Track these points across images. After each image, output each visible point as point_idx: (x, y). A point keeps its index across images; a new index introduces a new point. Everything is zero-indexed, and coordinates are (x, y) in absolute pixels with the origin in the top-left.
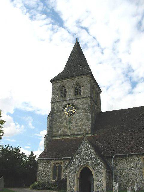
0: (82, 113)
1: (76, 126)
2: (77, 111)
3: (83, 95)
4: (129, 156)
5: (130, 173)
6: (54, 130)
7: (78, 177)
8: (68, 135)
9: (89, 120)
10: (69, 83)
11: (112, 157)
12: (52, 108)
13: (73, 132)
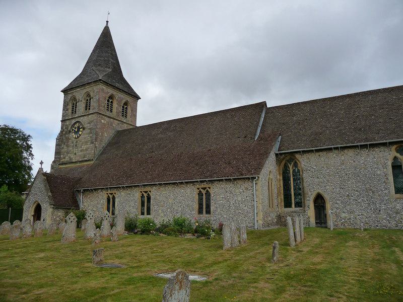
1: (81, 151)
2: (84, 132)
4: (95, 190)
5: (94, 209)
6: (62, 156)
7: (33, 214)
8: (73, 163)
12: (62, 128)
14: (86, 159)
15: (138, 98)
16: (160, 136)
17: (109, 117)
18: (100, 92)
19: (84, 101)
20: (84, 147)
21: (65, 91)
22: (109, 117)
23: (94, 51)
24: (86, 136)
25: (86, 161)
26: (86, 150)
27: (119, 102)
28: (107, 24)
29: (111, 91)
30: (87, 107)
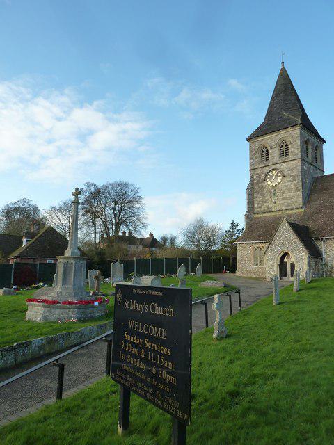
1: (283, 199)
3: (291, 157)
11: (322, 239)
19: (278, 148)
20: (286, 195)
26: (291, 198)
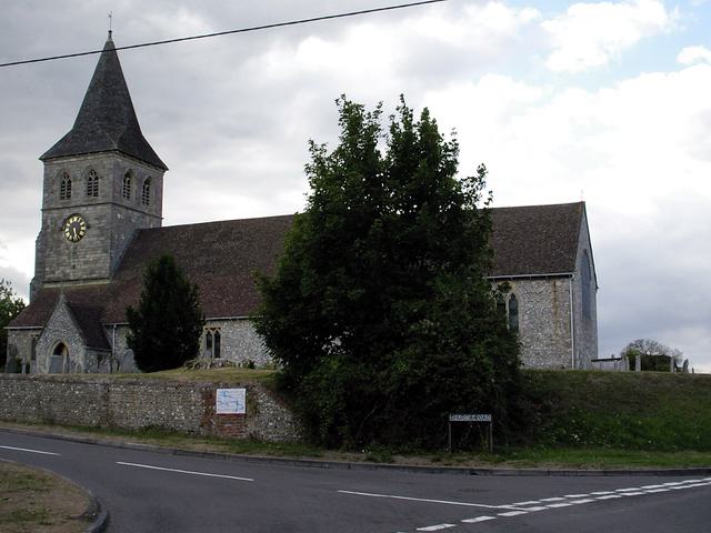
0: (94, 236)
1: (85, 263)
2: (89, 232)
3: (100, 199)
6: (47, 269)
9: (106, 252)
10: (76, 166)
12: (44, 222)
13: (79, 274)
14: (94, 276)
15: (165, 168)
16: (216, 246)
17: (127, 208)
18: (109, 165)
20: (90, 257)
21: (46, 158)
22: (127, 208)
23: (92, 89)
24: (91, 239)
25: (96, 279)
26: (95, 262)
27: (139, 181)
28: (110, 37)
29: (127, 164)
30: (92, 190)
